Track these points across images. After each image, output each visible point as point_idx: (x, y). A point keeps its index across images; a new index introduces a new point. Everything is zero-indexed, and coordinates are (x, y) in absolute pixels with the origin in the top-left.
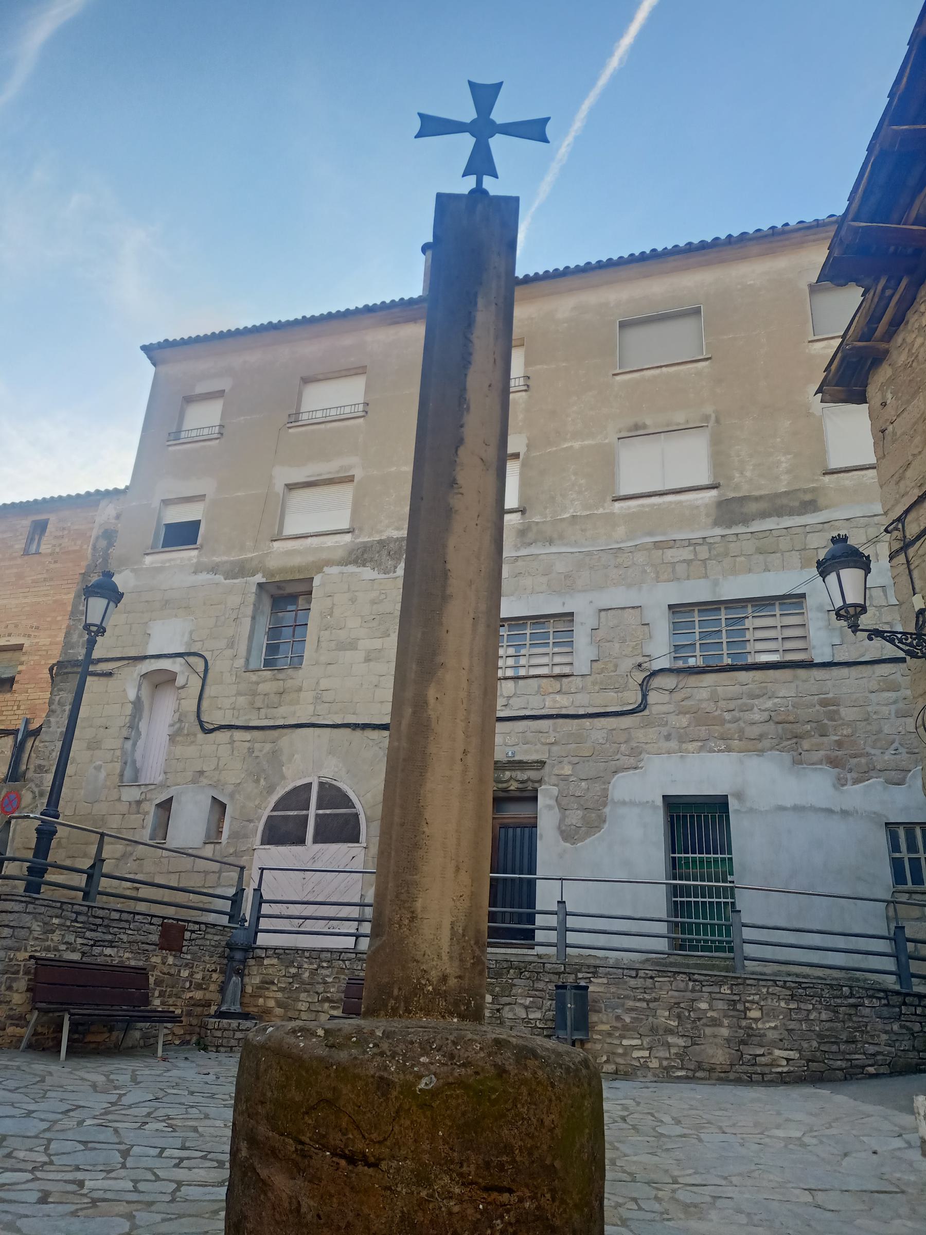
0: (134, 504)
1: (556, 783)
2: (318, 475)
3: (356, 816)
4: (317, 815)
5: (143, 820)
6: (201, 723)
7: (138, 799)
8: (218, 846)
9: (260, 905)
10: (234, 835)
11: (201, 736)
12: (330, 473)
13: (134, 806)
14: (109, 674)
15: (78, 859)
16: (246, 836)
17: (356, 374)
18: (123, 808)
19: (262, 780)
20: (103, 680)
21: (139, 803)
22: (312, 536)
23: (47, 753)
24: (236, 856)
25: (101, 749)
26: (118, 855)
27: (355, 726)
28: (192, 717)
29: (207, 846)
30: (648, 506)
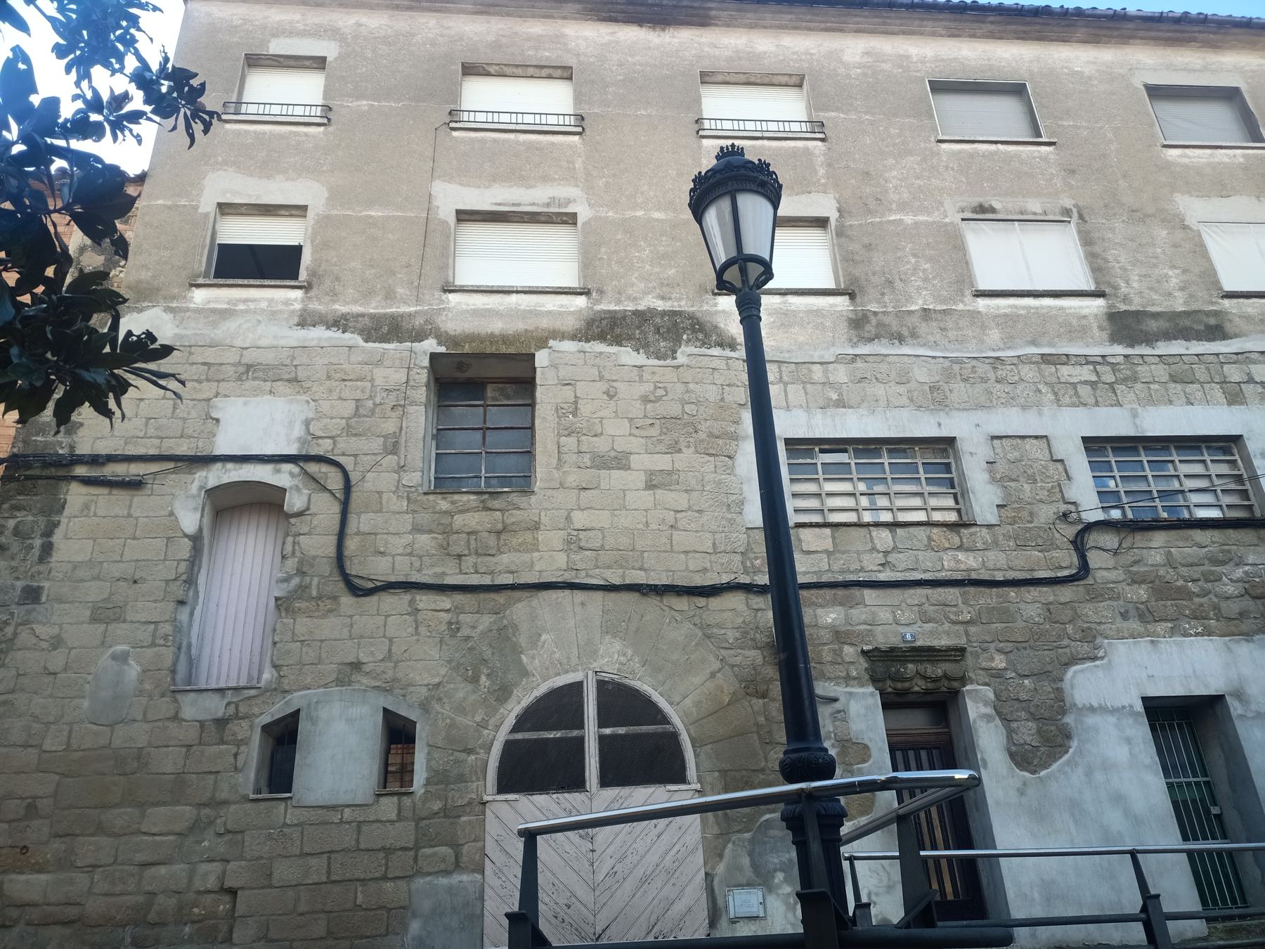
0: (160, 202)
2: (514, 205)
3: (674, 737)
4: (602, 739)
5: (236, 755)
7: (220, 714)
8: (407, 801)
10: (438, 778)
11: (347, 600)
12: (534, 204)
14: (135, 485)
15: (80, 839)
17: (550, 77)
19: (483, 678)
20: (121, 496)
21: (221, 723)
22: (518, 292)
24: (445, 816)
25: (124, 621)
26: (180, 826)
28: (326, 568)
29: (384, 800)
30: (1024, 308)
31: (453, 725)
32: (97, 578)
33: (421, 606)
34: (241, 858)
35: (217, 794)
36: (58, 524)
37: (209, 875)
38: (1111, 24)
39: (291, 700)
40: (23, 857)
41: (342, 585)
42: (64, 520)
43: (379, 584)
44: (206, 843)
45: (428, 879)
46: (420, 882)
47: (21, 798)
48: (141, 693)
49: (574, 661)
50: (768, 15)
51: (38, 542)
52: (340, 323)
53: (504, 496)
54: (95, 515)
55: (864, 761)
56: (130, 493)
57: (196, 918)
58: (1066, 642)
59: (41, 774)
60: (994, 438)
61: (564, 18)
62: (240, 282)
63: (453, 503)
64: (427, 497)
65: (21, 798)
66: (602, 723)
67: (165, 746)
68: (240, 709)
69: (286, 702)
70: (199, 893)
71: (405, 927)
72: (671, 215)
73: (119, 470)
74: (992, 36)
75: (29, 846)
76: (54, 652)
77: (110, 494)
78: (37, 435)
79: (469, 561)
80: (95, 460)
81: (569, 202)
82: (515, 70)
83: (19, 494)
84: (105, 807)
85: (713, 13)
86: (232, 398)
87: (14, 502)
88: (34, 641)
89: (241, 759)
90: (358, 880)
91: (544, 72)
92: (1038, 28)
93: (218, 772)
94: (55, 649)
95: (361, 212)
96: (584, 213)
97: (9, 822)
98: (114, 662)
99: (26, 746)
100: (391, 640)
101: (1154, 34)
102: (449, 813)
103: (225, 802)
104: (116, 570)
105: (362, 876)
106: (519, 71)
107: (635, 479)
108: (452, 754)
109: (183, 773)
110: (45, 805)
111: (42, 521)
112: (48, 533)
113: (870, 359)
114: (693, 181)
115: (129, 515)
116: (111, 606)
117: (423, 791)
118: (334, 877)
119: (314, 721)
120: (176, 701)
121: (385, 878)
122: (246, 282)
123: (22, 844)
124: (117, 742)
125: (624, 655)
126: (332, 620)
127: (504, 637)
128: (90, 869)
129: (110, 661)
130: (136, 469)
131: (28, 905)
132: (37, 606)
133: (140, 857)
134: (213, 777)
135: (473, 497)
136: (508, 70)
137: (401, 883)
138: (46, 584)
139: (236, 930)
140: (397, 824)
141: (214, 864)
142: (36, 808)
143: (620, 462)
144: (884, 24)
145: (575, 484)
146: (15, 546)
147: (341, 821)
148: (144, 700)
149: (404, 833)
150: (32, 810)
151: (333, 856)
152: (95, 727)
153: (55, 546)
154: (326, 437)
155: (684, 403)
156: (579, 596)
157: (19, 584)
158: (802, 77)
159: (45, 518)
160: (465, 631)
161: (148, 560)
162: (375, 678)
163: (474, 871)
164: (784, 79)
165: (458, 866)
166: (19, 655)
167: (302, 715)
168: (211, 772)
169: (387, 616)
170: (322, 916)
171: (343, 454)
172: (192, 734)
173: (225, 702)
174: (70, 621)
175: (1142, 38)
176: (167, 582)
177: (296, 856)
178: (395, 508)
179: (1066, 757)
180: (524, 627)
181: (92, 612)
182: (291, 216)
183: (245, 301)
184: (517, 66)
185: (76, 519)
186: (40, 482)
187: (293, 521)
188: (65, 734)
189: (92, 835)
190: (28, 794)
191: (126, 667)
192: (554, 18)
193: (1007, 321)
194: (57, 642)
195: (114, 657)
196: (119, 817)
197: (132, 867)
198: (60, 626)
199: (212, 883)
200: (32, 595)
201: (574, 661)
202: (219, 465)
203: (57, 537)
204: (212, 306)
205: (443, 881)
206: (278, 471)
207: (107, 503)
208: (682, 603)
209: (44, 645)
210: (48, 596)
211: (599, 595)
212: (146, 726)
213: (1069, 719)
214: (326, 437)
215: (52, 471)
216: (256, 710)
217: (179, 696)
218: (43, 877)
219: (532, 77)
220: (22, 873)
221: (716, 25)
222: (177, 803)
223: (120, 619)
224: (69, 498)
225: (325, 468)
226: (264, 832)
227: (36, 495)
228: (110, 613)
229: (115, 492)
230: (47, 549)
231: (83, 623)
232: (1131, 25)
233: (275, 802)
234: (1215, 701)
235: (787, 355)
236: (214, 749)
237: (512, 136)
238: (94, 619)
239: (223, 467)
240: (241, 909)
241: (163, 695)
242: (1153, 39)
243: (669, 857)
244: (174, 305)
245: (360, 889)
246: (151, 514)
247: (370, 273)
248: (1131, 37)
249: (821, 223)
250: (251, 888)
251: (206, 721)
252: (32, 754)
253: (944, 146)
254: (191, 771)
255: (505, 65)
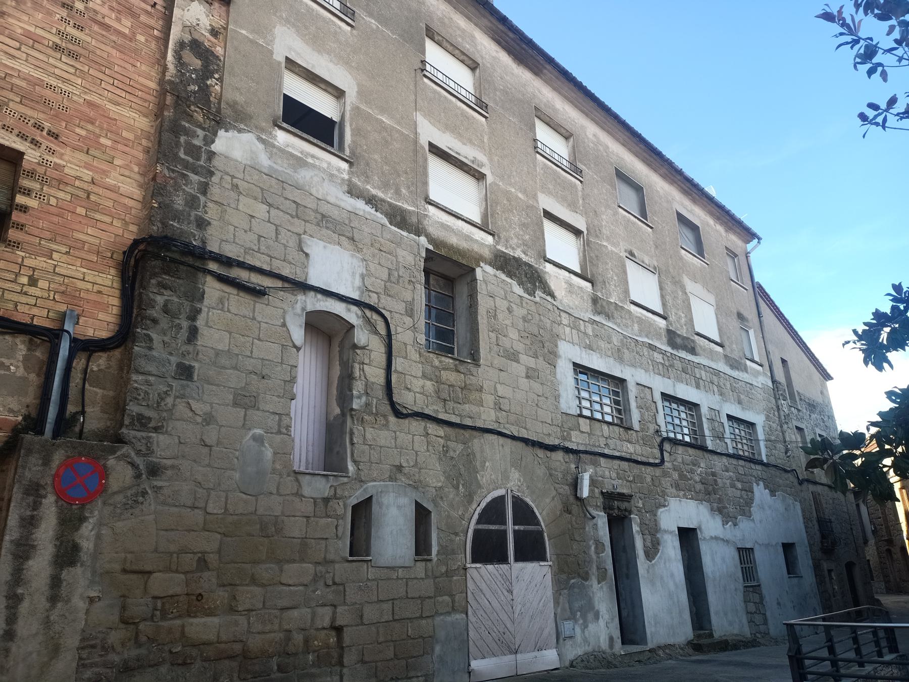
0: (244, 32)
1: (407, 392)
2: (457, 153)
3: (541, 533)
4: (515, 532)
5: (337, 527)
6: (392, 404)
7: (326, 495)
8: (429, 564)
9: (724, 645)
10: (443, 550)
11: (392, 419)
12: (466, 157)
13: (321, 505)
14: (258, 293)
15: (239, 588)
16: (453, 552)
17: (462, 62)
18: (307, 507)
19: (461, 487)
20: (246, 298)
21: (326, 500)
22: (463, 220)
23: (153, 397)
24: (447, 576)
25: (258, 409)
26: (307, 579)
27: (526, 441)
28: (380, 393)
29: (418, 564)
30: (645, 317)
31: (449, 516)
32: (235, 368)
33: (430, 431)
34: (345, 603)
35: (328, 556)
36: (199, 311)
37: (325, 616)
38: (674, 173)
39: (367, 488)
40: (198, 603)
41: (389, 407)
42: (205, 309)
43: (410, 412)
44: (318, 592)
45: (442, 617)
46: (438, 620)
47: (194, 553)
48: (274, 471)
49: (500, 482)
50: (566, 89)
51: (185, 324)
52: (371, 201)
53: (466, 364)
54: (229, 311)
55: (603, 552)
56: (254, 298)
57: (317, 649)
58: (657, 496)
59: (207, 533)
60: (638, 384)
61: (476, 25)
62: (311, 139)
63: (441, 362)
64: (429, 354)
65: (194, 553)
66: (514, 524)
67: (294, 516)
68: (338, 491)
69: (364, 490)
70: (317, 629)
71: (433, 650)
72: (526, 199)
73: (243, 275)
74: (636, 155)
75: (203, 594)
76: (207, 427)
77: (238, 295)
78: (174, 220)
79: (451, 404)
80: (228, 262)
81: (482, 165)
82: (449, 46)
83: (165, 274)
84: (255, 562)
85: (545, 71)
86: (315, 239)
87: (160, 279)
88: (190, 414)
89: (340, 529)
90: (408, 619)
91: (462, 57)
92: (652, 160)
93: (327, 539)
94: (208, 424)
95: (377, 115)
96: (490, 178)
97: (185, 573)
98: (254, 443)
99: (194, 507)
100: (416, 452)
101: (683, 185)
102: (448, 574)
103: (333, 562)
104: (249, 364)
105: (410, 616)
106: (450, 48)
107: (518, 369)
108: (449, 536)
109: (306, 538)
110: (212, 559)
111: (187, 306)
112: (193, 315)
113: (599, 324)
114: (873, 314)
115: (254, 319)
116: (248, 395)
117: (436, 559)
118: (396, 617)
119: (380, 505)
120: (297, 480)
121: (421, 617)
122: (315, 141)
123: (198, 592)
124: (260, 511)
125: (520, 481)
126: (384, 434)
127: (469, 458)
128: (246, 613)
129: (251, 441)
130: (267, 282)
131: (204, 644)
132: (189, 383)
133: (282, 603)
134: (323, 542)
135: (451, 361)
136: (445, 44)
137: (429, 620)
138: (196, 365)
139: (345, 656)
140: (425, 581)
141: (327, 608)
142: (205, 561)
143: (513, 356)
144: (605, 123)
145: (497, 366)
146: (164, 323)
147: (398, 578)
148: (277, 477)
149: (427, 588)
150: (203, 564)
151: (395, 602)
152: (244, 496)
153: (200, 331)
154: (374, 292)
155: (539, 327)
156: (502, 440)
157: (173, 359)
158: (571, 135)
159: (190, 303)
160: (451, 453)
161: (270, 360)
162: (408, 478)
163: (462, 612)
164: (563, 131)
165: (454, 610)
166: (178, 424)
167: (374, 499)
168: (323, 539)
169: (414, 435)
170: (391, 644)
171: (384, 309)
172: (308, 508)
173: (329, 485)
174: (218, 402)
175: (678, 185)
176: (285, 381)
177: (375, 602)
178: (414, 358)
179: (659, 555)
180: (478, 455)
181: (234, 397)
182: (325, 90)
183: (313, 156)
184: (452, 45)
185: (214, 311)
186: (181, 267)
187: (358, 351)
188: (223, 499)
189: (247, 585)
190: (199, 550)
191: (263, 449)
192: (471, 21)
193: (640, 321)
194: (209, 419)
195: (255, 438)
196: (265, 571)
197: (276, 611)
198: (211, 404)
199: (326, 622)
200: (185, 372)
201: (500, 482)
202: (312, 293)
203: (200, 322)
204: (290, 150)
205: (449, 619)
206: (349, 310)
207: (238, 302)
208: (541, 453)
209: (199, 419)
210: (198, 375)
211: (509, 441)
212: (280, 499)
213: (658, 536)
214: (374, 292)
215: (190, 260)
216: (346, 493)
217: (300, 477)
218: (215, 620)
219: (453, 55)
220: (195, 617)
221: (541, 78)
222: (302, 561)
223: (255, 407)
224: (206, 289)
225: (375, 317)
226: (357, 584)
227: (179, 278)
228: (247, 400)
229: (242, 294)
230: (194, 332)
231: (228, 405)
232: (679, 177)
233: (361, 563)
234: (694, 530)
235: (571, 310)
236: (323, 521)
237: (454, 99)
238: (236, 404)
239: (315, 295)
240: (347, 640)
241: (288, 476)
242: (682, 188)
243: (541, 604)
244: (264, 137)
245: (410, 624)
246: (269, 321)
247: (386, 168)
248: (675, 182)
249: (577, 232)
250: (352, 626)
251: (317, 498)
252: (199, 515)
253: (620, 210)
254: (311, 537)
255: (447, 40)
